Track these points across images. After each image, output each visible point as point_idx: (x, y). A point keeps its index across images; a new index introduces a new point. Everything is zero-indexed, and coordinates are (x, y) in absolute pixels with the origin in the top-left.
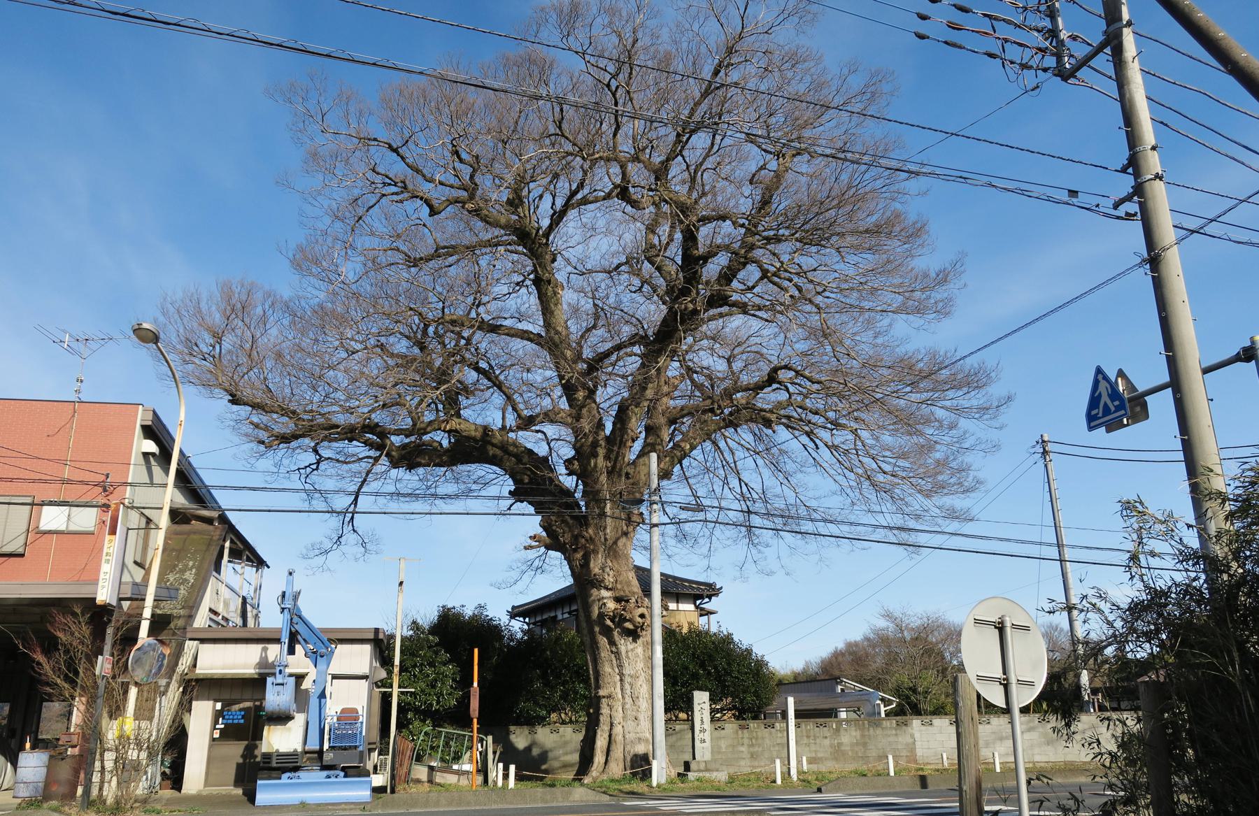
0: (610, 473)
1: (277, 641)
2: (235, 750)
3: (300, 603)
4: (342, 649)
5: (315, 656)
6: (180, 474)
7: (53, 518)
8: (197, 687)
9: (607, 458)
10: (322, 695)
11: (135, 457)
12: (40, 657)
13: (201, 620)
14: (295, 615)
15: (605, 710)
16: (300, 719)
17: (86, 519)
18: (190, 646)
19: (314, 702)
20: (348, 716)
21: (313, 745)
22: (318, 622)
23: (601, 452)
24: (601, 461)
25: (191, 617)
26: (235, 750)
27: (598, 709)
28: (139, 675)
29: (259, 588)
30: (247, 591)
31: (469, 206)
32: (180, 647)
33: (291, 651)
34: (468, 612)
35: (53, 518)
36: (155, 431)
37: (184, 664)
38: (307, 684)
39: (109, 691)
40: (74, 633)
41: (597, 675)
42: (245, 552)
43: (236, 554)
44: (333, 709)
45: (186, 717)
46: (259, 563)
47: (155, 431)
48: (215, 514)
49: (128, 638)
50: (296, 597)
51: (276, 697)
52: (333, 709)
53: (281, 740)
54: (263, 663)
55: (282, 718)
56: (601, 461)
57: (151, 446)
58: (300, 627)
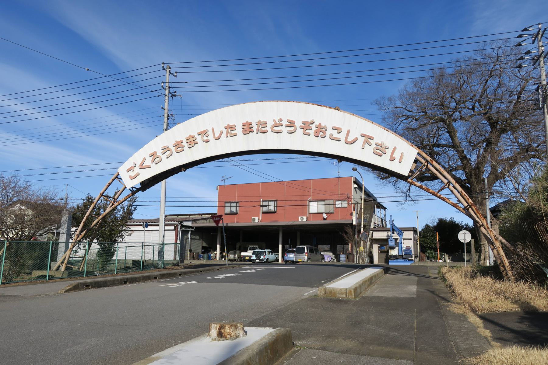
0: (477, 182)
1: (390, 231)
2: (384, 255)
3: (394, 222)
4: (405, 233)
5: (399, 234)
6: (365, 191)
7: (338, 204)
8: (374, 241)
9: (475, 178)
10: (401, 243)
11: (353, 190)
12: (344, 235)
13: (372, 226)
14: (393, 225)
15: (483, 248)
16: (397, 248)
17: (345, 204)
18: (371, 232)
19: (400, 244)
20: (408, 248)
21: (400, 254)
22: (398, 226)
23: (473, 177)
24: (473, 179)
25: (370, 225)
26: (384, 255)
27: (481, 248)
28: (363, 239)
29: (385, 215)
30: (382, 216)
31: (426, 117)
32: (369, 232)
33: (393, 233)
34: (448, 219)
35: (338, 204)
36: (356, 182)
37: (370, 236)
38: (398, 241)
39: (358, 242)
40: (349, 231)
41: (480, 238)
42: (380, 206)
43: (378, 207)
44: (404, 246)
45: (372, 249)
46: (385, 208)
47: (356, 182)
48: (372, 199)
49: (360, 231)
50: (393, 221)
51: (391, 243)
52: (404, 246)
53: (394, 252)
54: (388, 236)
55: (393, 248)
56: (473, 179)
57: (356, 186)
58: (394, 228)
